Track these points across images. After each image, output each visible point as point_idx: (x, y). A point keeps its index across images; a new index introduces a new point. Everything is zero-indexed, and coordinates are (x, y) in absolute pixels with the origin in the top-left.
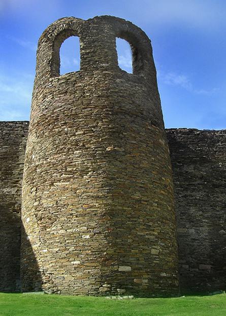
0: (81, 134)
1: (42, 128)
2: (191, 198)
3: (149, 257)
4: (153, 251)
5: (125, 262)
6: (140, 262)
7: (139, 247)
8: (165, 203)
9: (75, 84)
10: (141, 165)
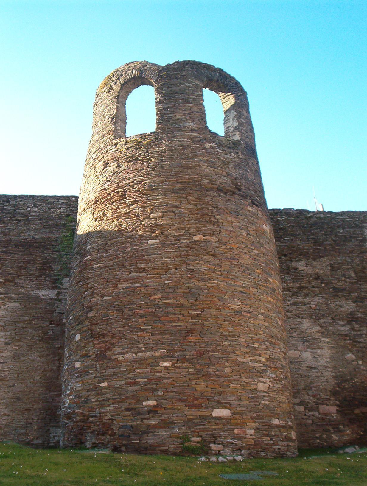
0: (157, 217)
1: (102, 207)
2: (304, 307)
3: (255, 396)
4: (261, 387)
5: (222, 403)
6: (242, 403)
7: (241, 380)
8: (274, 315)
9: (148, 149)
10: (240, 261)
